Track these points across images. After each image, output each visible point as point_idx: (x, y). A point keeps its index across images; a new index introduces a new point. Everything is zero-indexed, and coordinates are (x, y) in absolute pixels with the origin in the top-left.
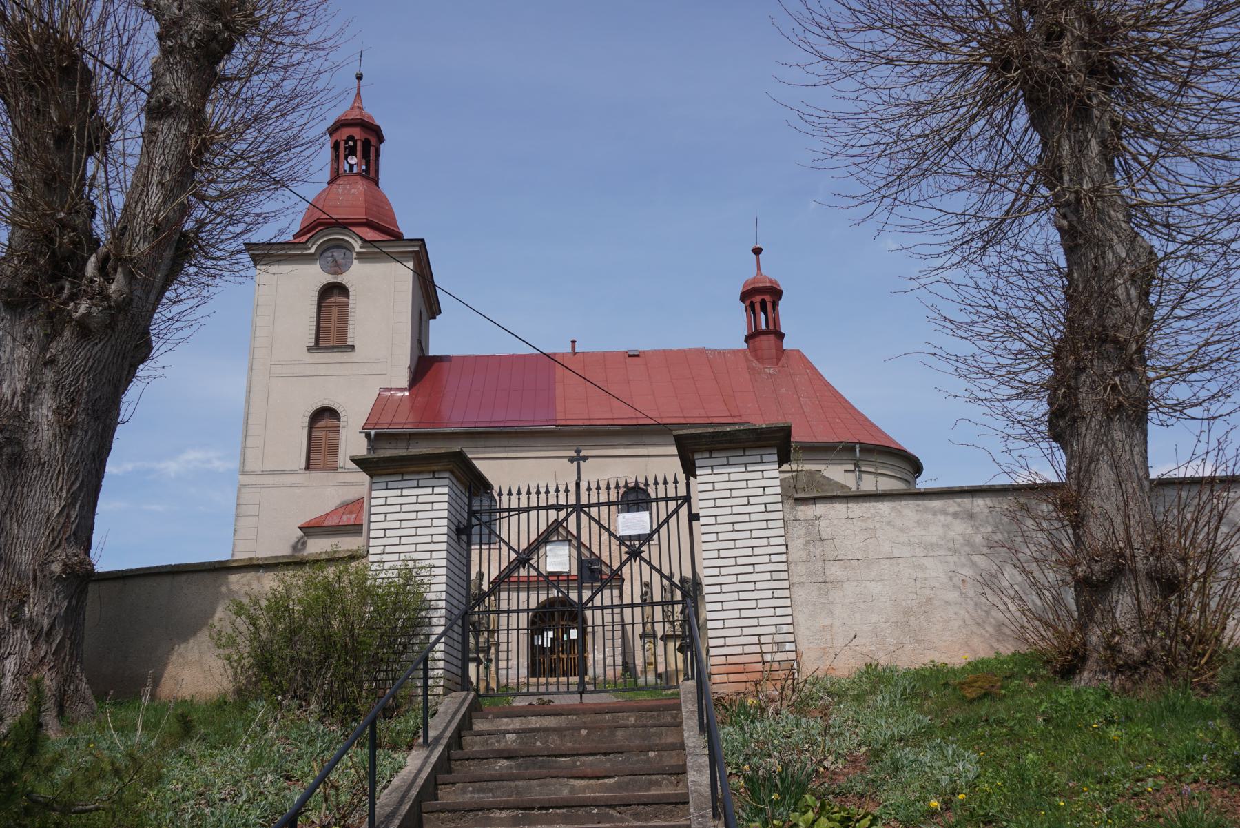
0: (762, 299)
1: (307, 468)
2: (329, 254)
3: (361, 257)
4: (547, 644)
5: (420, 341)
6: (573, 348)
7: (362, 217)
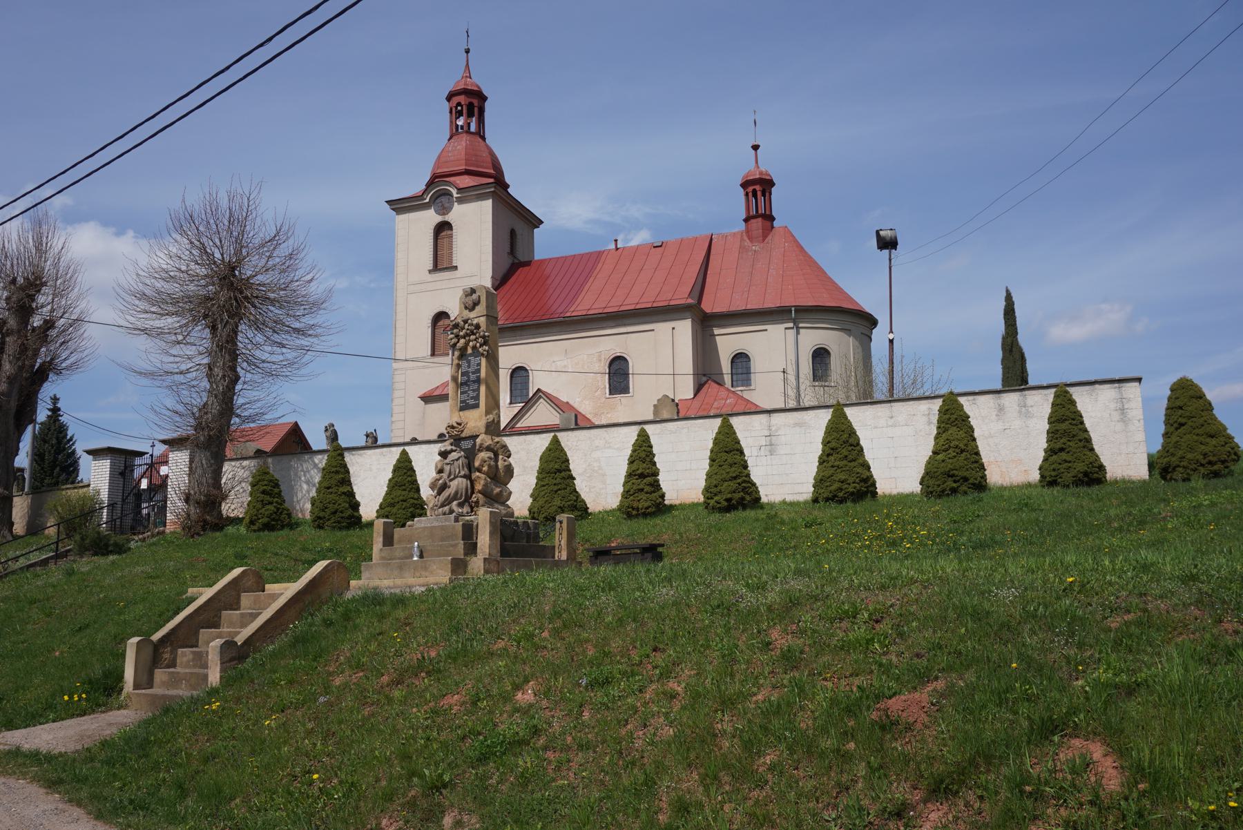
0: (759, 188)
1: (433, 354)
3: (461, 201)
5: (141, 373)
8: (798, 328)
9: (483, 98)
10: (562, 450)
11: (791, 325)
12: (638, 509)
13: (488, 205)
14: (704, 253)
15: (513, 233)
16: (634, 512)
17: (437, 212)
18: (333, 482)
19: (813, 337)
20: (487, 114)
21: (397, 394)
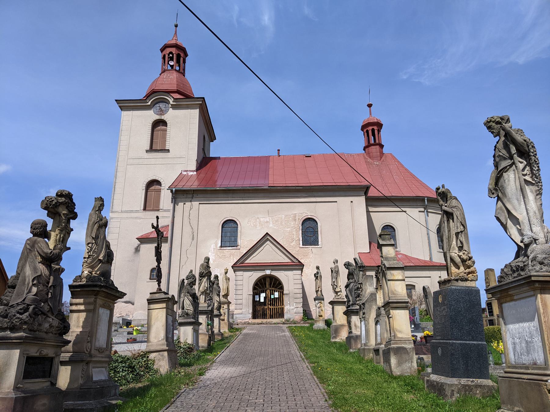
0: (372, 129)
1: (145, 209)
2: (157, 105)
3: (174, 107)
4: (262, 300)
5: (204, 150)
6: (279, 153)
7: (175, 88)
8: (427, 212)
11: (422, 209)
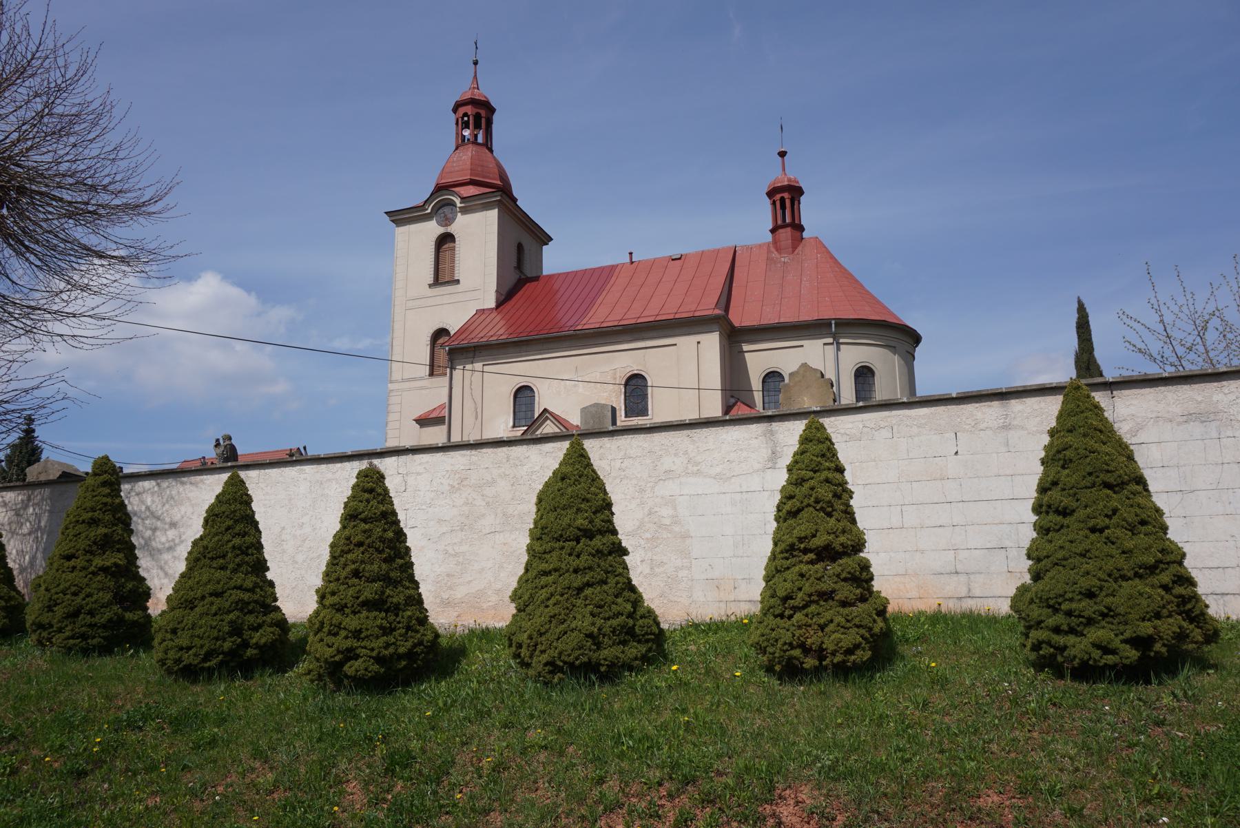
0: (786, 199)
1: (431, 374)
3: (465, 211)
8: (838, 344)
9: (492, 110)
10: (595, 478)
11: (830, 340)
12: (821, 653)
13: (493, 214)
14: (728, 265)
15: (520, 248)
16: (810, 662)
17: (439, 223)
18: (82, 544)
19: (855, 354)
20: (494, 127)
21: (392, 417)
